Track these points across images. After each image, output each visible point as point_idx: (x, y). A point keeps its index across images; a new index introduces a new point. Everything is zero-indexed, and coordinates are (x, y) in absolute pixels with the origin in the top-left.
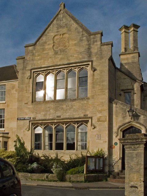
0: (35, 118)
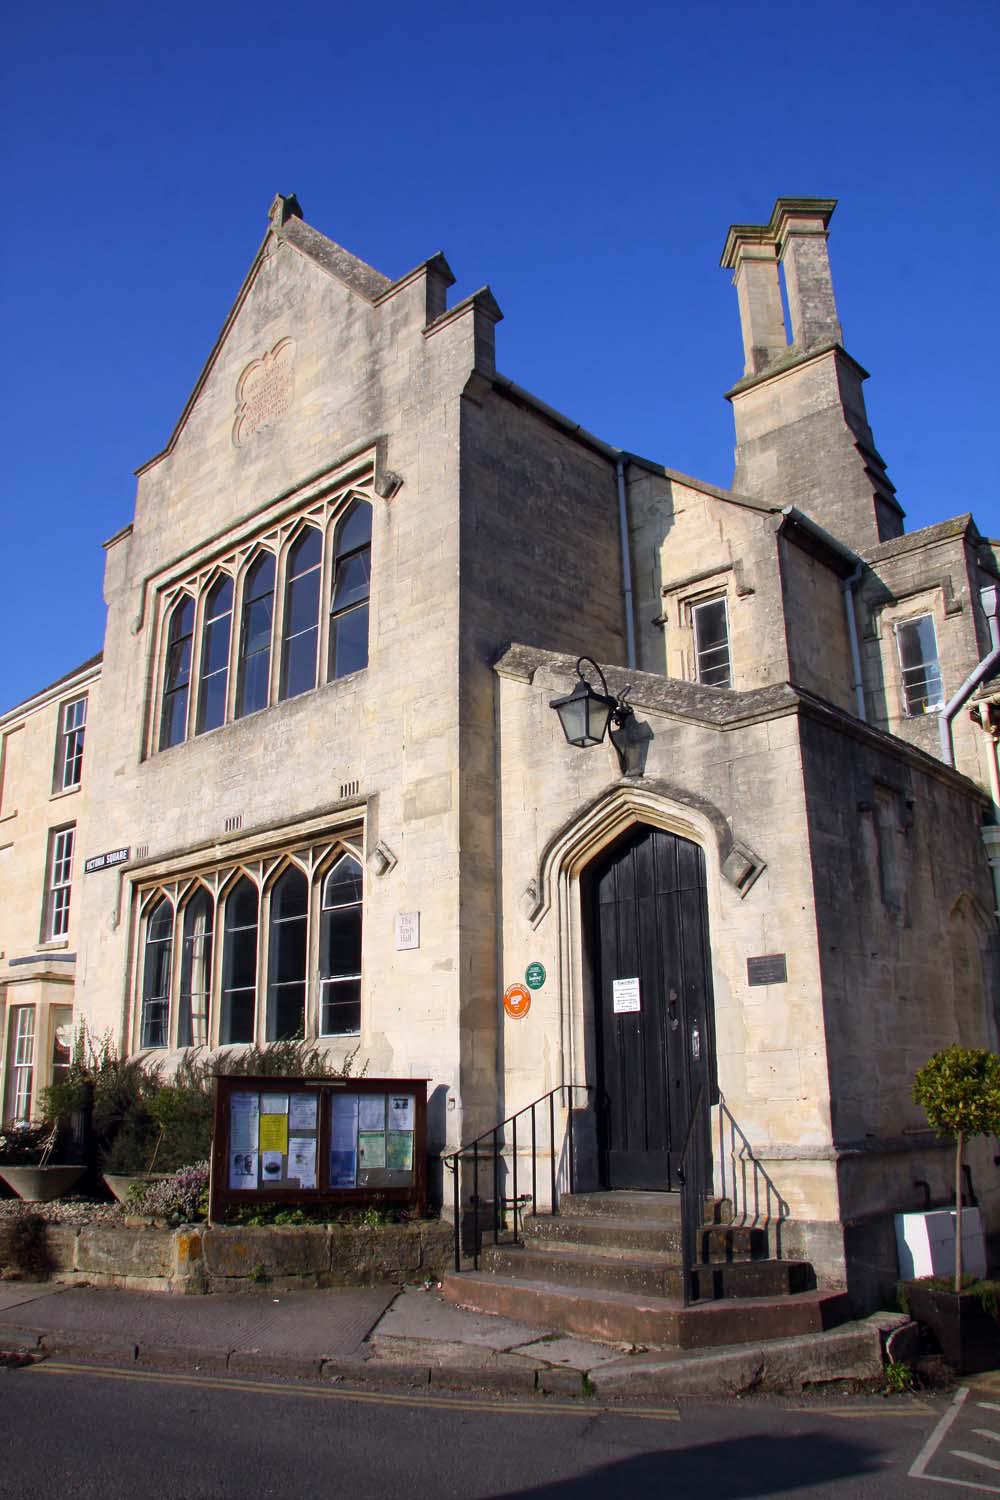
0: (146, 850)
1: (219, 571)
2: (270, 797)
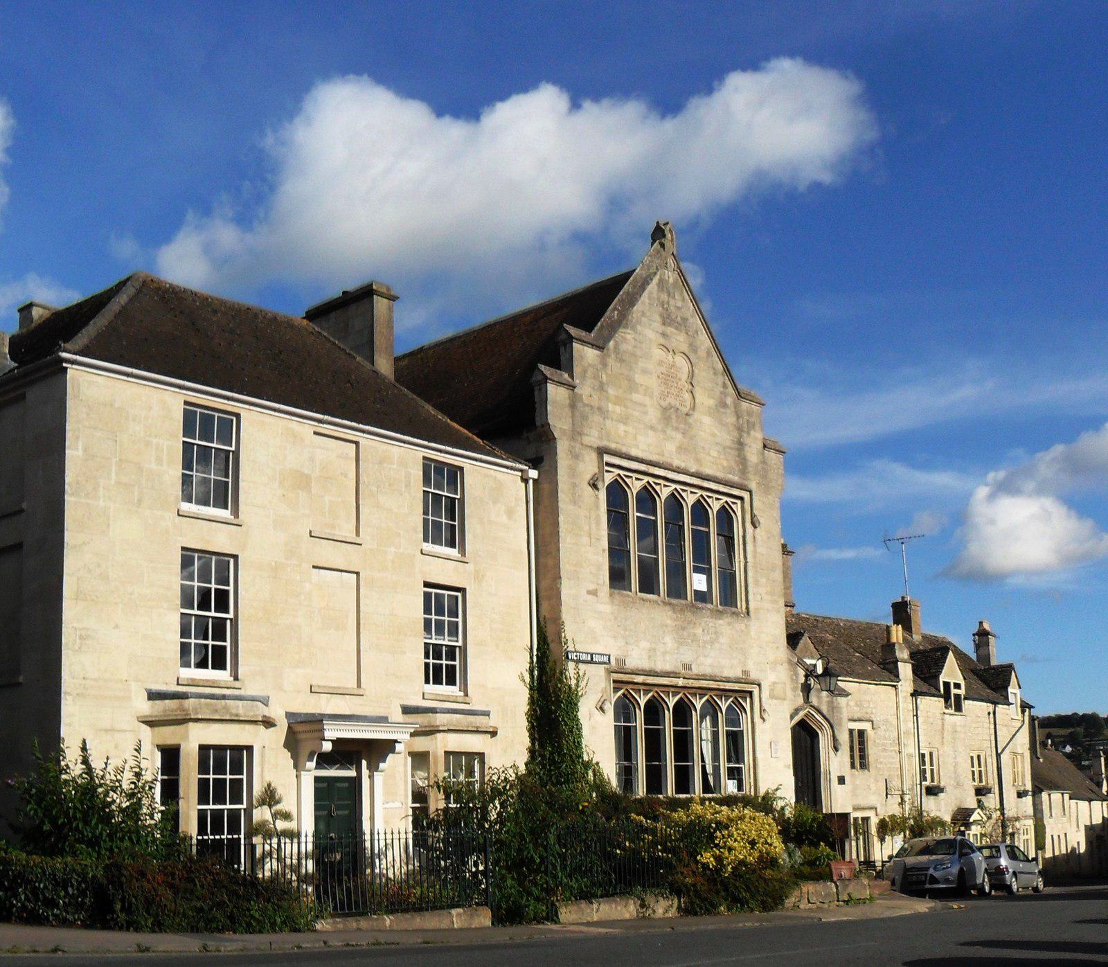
1: (459, 594)
2: (709, 661)
